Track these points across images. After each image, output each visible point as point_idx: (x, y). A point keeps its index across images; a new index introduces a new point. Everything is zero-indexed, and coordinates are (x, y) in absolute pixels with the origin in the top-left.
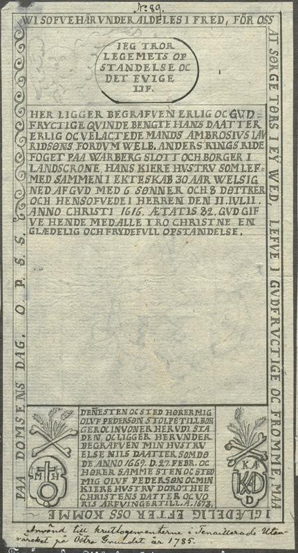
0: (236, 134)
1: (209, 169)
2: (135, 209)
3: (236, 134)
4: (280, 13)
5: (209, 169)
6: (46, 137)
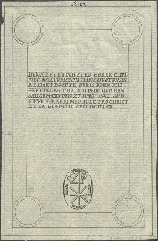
0: (101, 79)
1: (116, 80)
2: (100, 94)
3: (101, 79)
4: (151, 6)
5: (116, 80)
6: (85, 91)
